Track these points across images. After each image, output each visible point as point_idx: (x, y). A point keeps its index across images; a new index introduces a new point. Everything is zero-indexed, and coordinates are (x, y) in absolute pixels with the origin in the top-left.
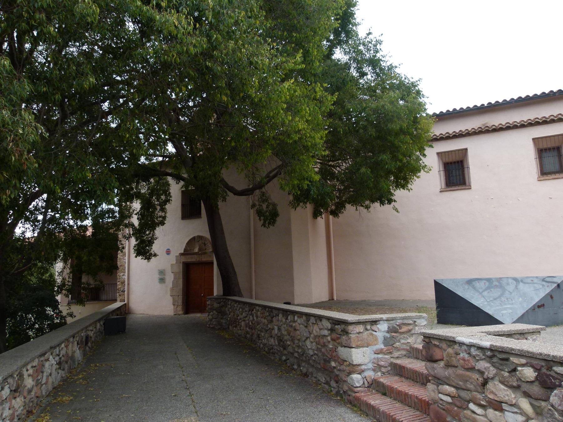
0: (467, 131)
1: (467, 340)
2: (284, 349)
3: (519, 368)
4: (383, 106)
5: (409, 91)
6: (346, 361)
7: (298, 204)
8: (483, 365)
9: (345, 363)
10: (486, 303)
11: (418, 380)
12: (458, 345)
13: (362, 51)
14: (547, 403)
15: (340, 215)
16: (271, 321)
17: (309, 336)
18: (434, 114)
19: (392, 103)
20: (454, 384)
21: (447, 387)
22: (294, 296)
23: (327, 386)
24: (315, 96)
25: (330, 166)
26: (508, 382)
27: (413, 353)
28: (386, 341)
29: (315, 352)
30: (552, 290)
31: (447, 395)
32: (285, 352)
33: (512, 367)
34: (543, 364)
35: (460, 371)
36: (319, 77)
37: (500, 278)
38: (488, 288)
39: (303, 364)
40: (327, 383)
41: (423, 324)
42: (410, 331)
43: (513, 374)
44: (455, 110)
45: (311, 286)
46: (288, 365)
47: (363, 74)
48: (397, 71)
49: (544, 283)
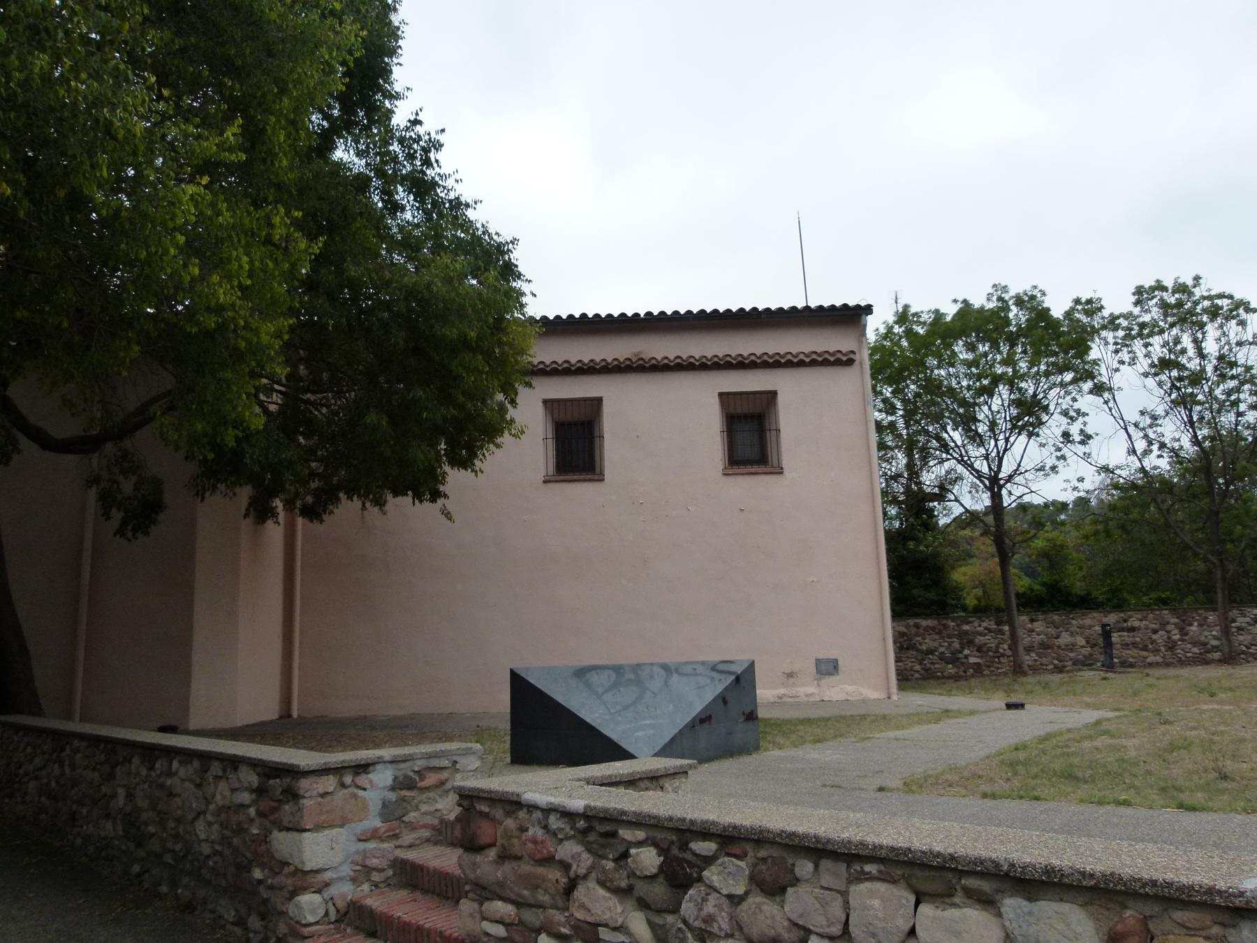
0: (566, 365)
1: (542, 799)
2: (139, 845)
3: (633, 851)
4: (428, 286)
5: (493, 260)
6: (288, 864)
7: (214, 488)
8: (570, 850)
9: (286, 870)
10: (607, 717)
11: (450, 895)
12: (525, 810)
13: (397, 157)
14: (676, 916)
15: (325, 517)
16: (111, 777)
17: (203, 807)
18: (544, 318)
19: (448, 280)
20: (512, 896)
21: (500, 903)
22: (187, 710)
23: (238, 931)
24: (269, 235)
25: (307, 402)
26: (611, 881)
27: (442, 834)
28: (387, 811)
29: (218, 847)
30: (726, 689)
31: (497, 922)
32: (142, 853)
33: (621, 849)
34: (674, 838)
35: (526, 868)
36: (291, 195)
37: (639, 665)
38: (615, 686)
39: (185, 880)
40: (241, 922)
41: (472, 767)
42: (442, 783)
43: (622, 863)
44: (584, 316)
45: (236, 679)
46: (146, 885)
47: (395, 208)
48: (470, 213)
49: (714, 674)
